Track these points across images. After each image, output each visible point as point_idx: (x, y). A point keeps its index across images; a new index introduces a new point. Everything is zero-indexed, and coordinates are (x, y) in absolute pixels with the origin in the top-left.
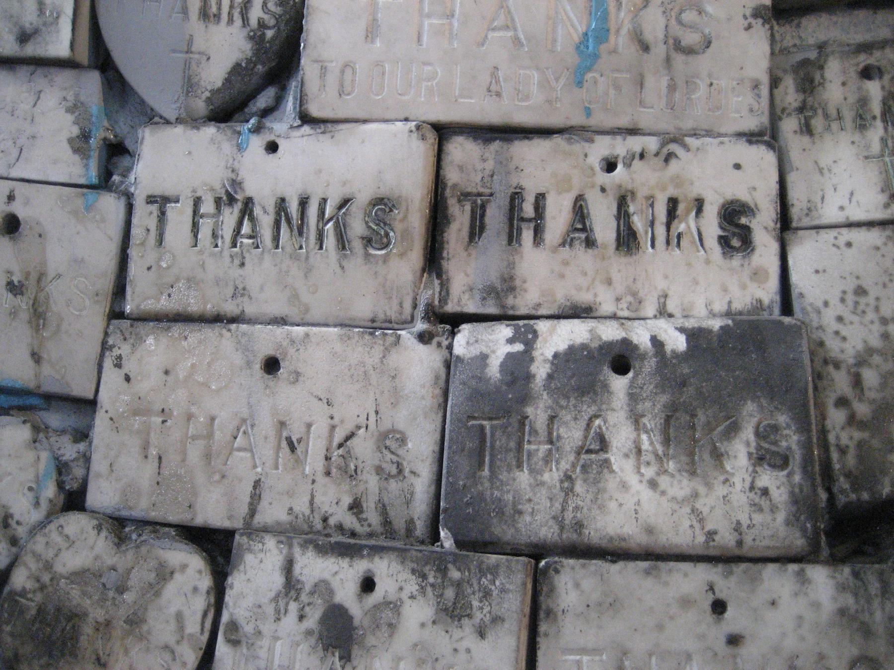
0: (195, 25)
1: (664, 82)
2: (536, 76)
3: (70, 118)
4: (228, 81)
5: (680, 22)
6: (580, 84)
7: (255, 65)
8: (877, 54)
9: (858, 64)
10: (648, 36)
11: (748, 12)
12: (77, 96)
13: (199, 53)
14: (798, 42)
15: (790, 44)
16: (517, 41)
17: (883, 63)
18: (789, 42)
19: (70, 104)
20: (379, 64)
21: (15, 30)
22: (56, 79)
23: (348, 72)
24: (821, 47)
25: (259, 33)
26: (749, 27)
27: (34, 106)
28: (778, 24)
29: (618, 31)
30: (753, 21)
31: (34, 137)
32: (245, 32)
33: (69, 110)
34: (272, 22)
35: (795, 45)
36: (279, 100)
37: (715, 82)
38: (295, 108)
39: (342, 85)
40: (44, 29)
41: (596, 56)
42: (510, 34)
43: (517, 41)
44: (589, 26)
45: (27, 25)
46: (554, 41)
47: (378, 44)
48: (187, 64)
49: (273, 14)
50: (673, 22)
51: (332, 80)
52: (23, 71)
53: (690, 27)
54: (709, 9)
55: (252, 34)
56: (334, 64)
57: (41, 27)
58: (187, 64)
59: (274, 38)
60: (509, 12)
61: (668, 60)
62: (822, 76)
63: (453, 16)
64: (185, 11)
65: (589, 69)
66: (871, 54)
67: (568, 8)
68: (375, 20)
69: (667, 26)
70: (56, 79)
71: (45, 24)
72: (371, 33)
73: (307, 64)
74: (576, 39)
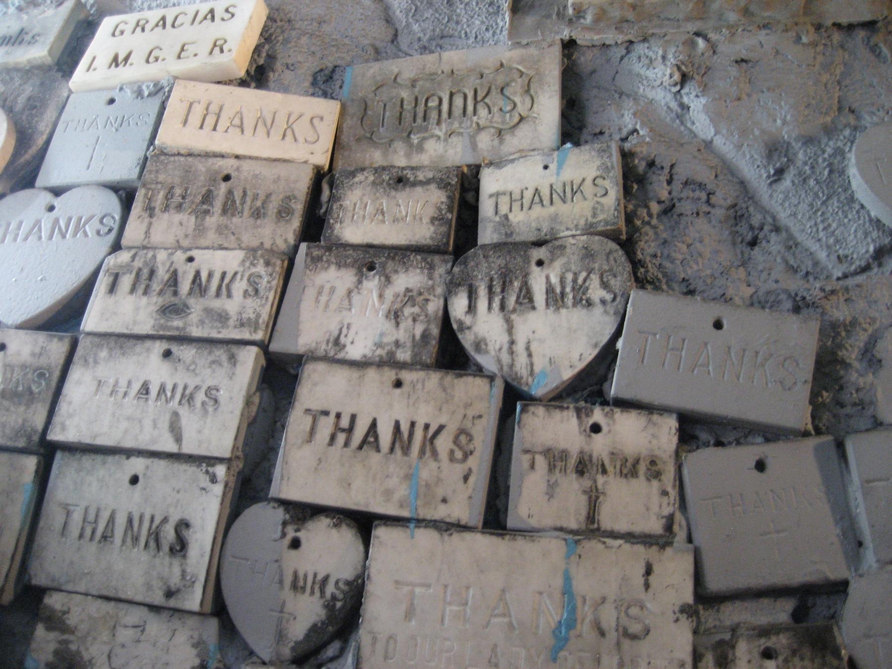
0: (287, 593)
1: (615, 660)
2: (523, 652)
3: (194, 652)
4: (308, 636)
5: (627, 615)
6: (555, 660)
7: (327, 627)
8: (774, 639)
9: (760, 646)
10: (604, 625)
11: (677, 609)
12: (200, 635)
13: (289, 614)
14: (717, 623)
15: (712, 625)
16: (511, 626)
17: (778, 647)
18: (711, 623)
19: (195, 641)
20: (413, 638)
21: (165, 587)
22: (187, 621)
23: (391, 642)
24: (734, 630)
25: (332, 604)
26: (677, 620)
27: (171, 639)
28: (704, 609)
29: (583, 620)
30: (680, 616)
31: (167, 664)
32: (322, 601)
33: (195, 646)
34: (341, 596)
35: (715, 627)
36: (342, 651)
37: (652, 661)
38: (353, 663)
39: (386, 652)
40: (184, 589)
41: (567, 639)
42: (506, 620)
43: (511, 626)
44: (562, 616)
45: (172, 585)
46: (537, 627)
47: (413, 623)
48: (280, 621)
49: (342, 591)
50: (623, 614)
51: (380, 647)
52: (165, 615)
53: (635, 619)
54: (649, 605)
55: (326, 603)
56: (382, 636)
57: (182, 588)
58: (280, 621)
59: (343, 607)
60: (506, 603)
61: (618, 644)
62: (734, 655)
63: (466, 604)
64: (281, 582)
65: (561, 649)
66: (770, 638)
67: (548, 602)
68: (412, 604)
69: (618, 618)
70: (187, 621)
71: (184, 586)
72: (409, 614)
73: (363, 634)
74: (553, 625)
